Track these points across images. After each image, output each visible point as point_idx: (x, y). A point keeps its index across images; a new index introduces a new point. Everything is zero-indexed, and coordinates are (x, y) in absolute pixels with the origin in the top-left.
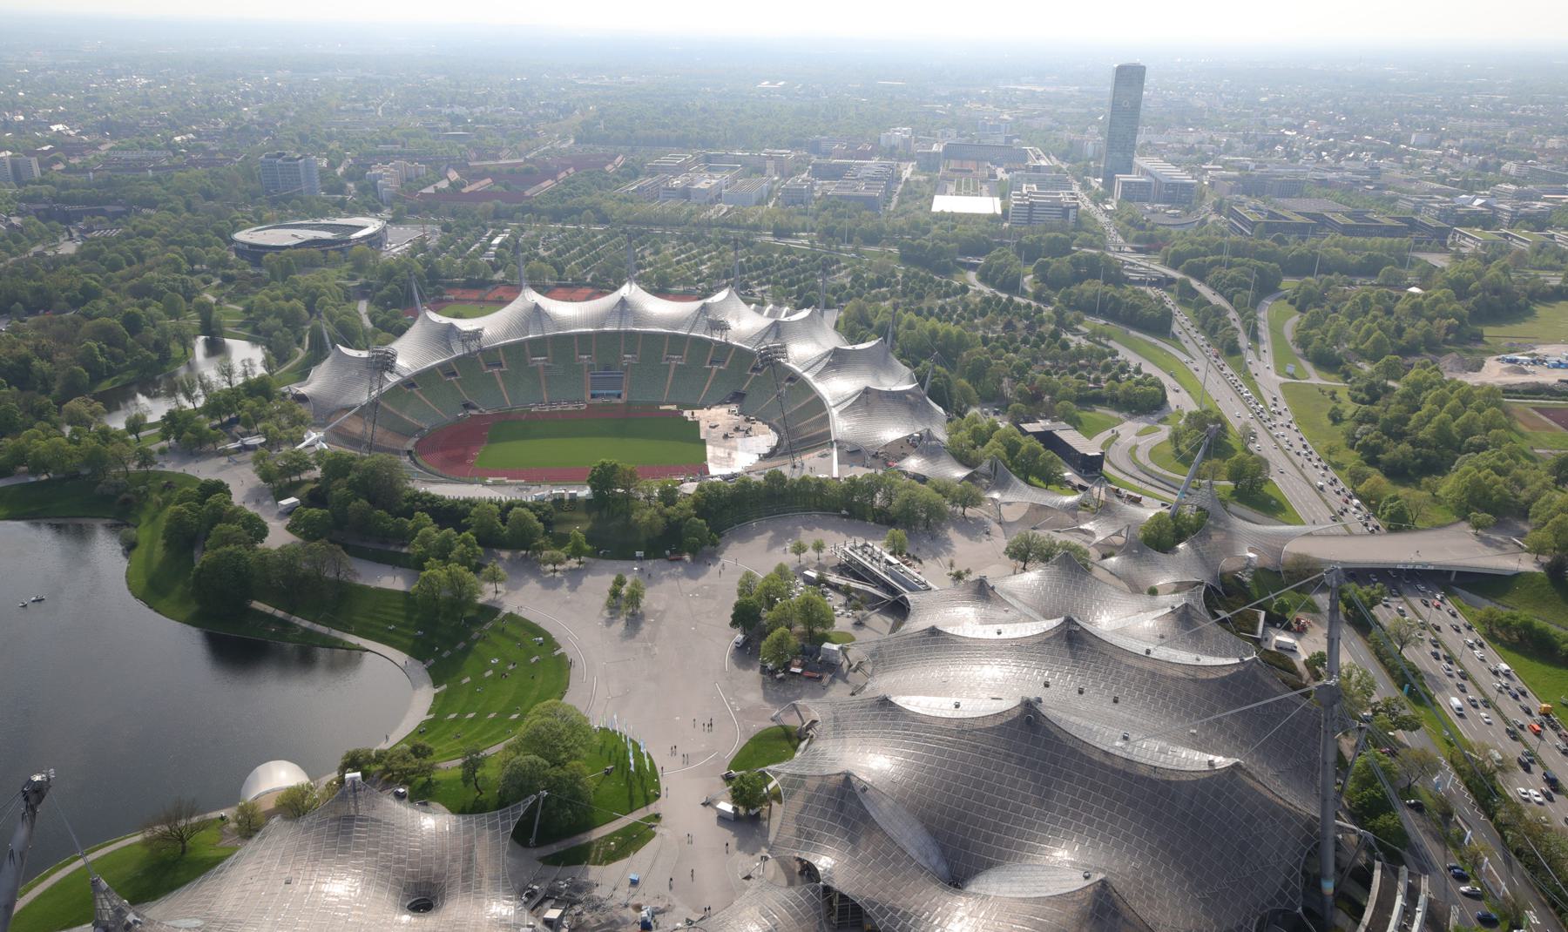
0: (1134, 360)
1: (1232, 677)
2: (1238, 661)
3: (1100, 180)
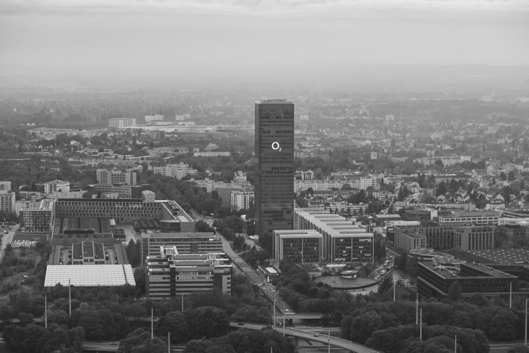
3: (256, 237)
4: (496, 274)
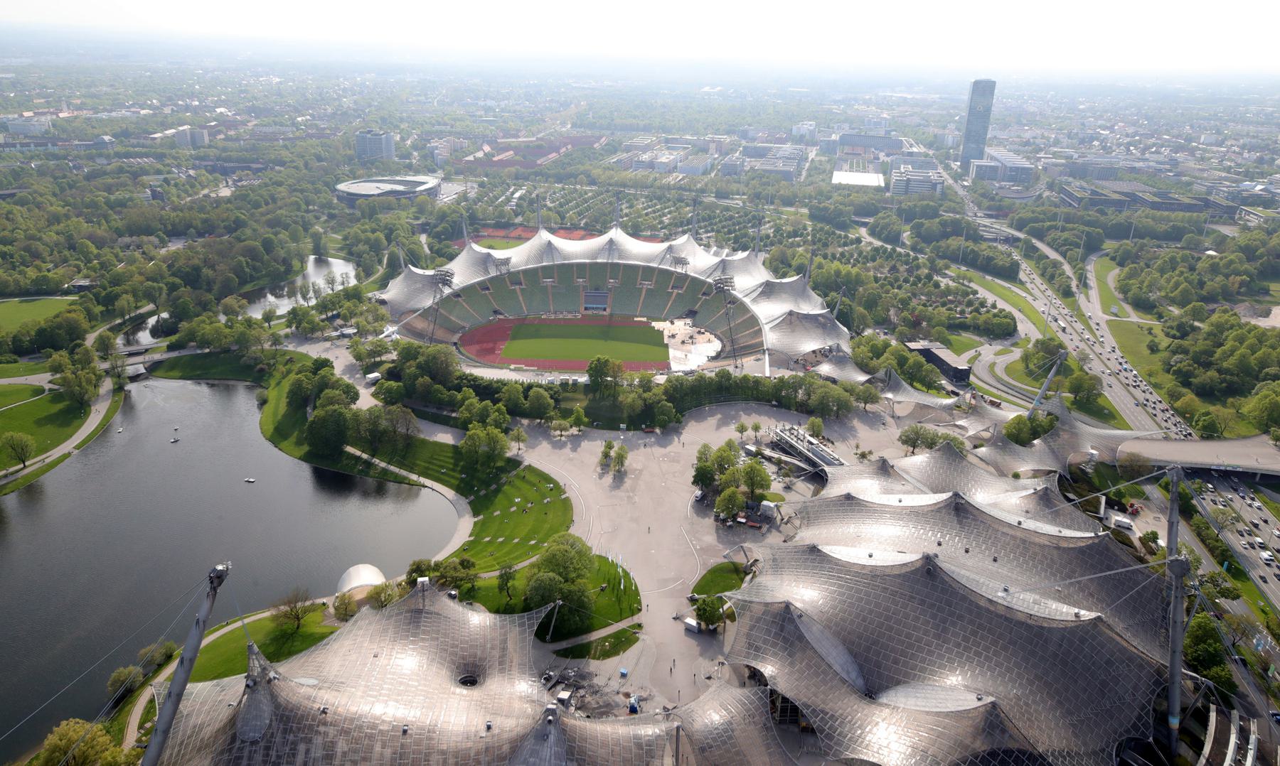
0: (990, 298)
1: (1089, 547)
2: (1093, 535)
3: (959, 163)
4: (1116, 197)
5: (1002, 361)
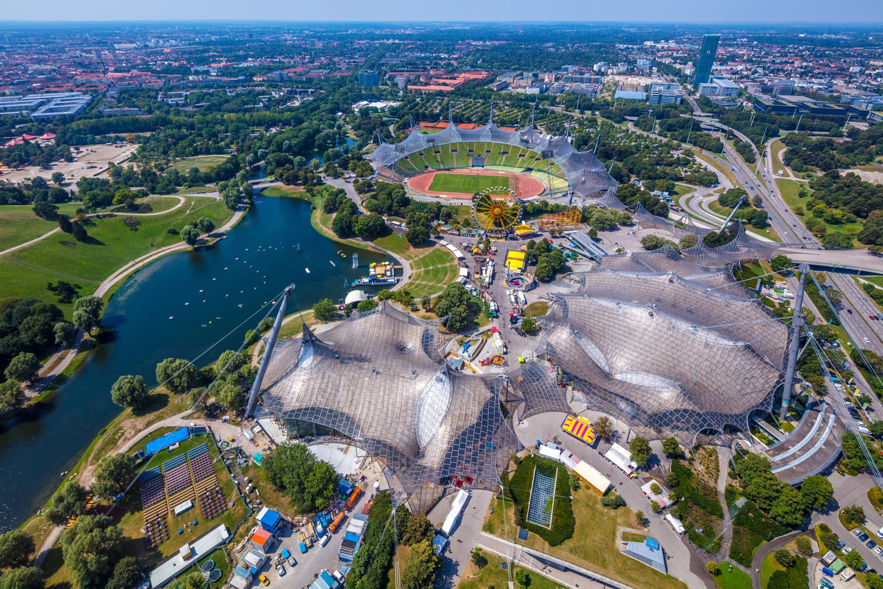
0: (704, 164)
4: (790, 105)
5: (707, 200)
